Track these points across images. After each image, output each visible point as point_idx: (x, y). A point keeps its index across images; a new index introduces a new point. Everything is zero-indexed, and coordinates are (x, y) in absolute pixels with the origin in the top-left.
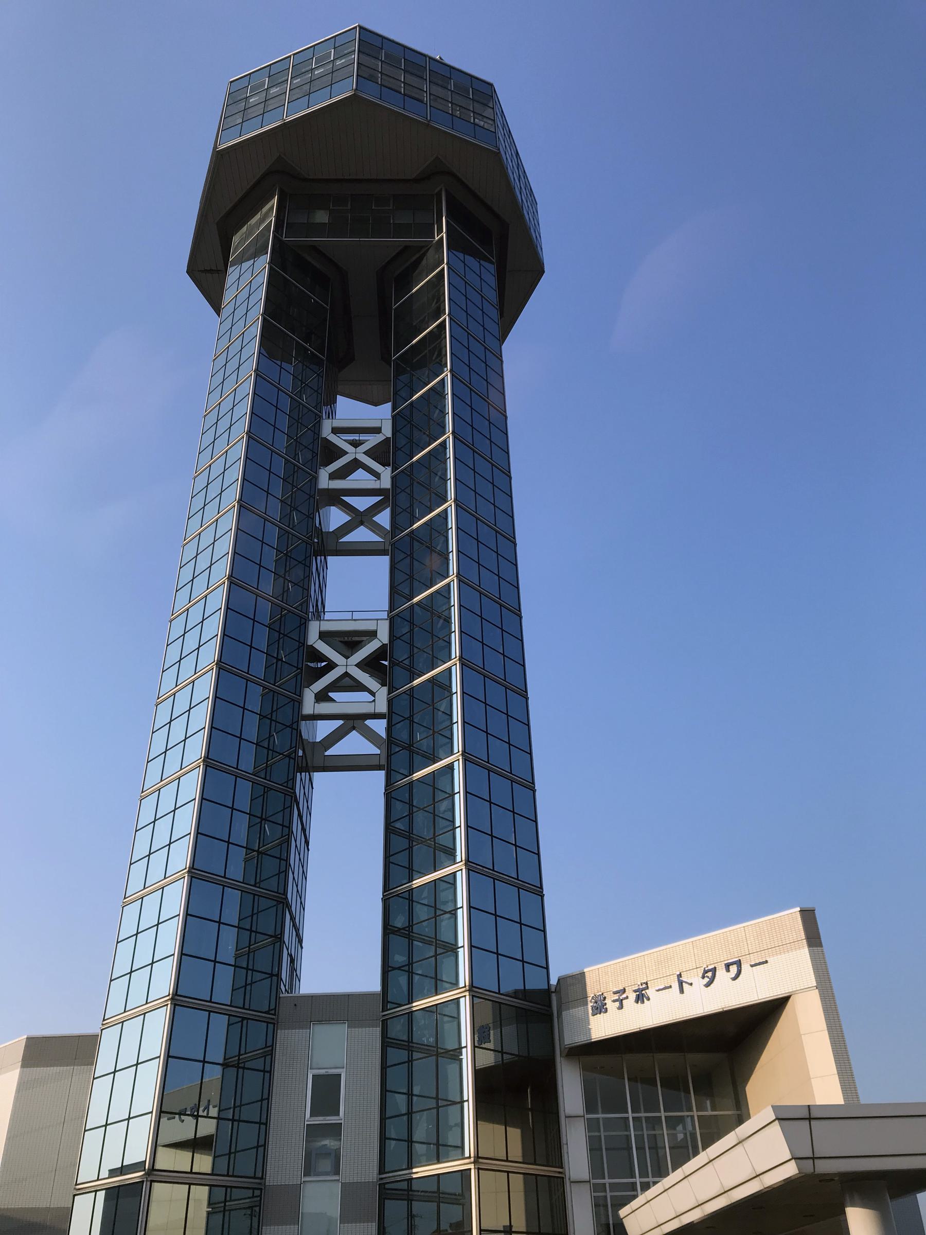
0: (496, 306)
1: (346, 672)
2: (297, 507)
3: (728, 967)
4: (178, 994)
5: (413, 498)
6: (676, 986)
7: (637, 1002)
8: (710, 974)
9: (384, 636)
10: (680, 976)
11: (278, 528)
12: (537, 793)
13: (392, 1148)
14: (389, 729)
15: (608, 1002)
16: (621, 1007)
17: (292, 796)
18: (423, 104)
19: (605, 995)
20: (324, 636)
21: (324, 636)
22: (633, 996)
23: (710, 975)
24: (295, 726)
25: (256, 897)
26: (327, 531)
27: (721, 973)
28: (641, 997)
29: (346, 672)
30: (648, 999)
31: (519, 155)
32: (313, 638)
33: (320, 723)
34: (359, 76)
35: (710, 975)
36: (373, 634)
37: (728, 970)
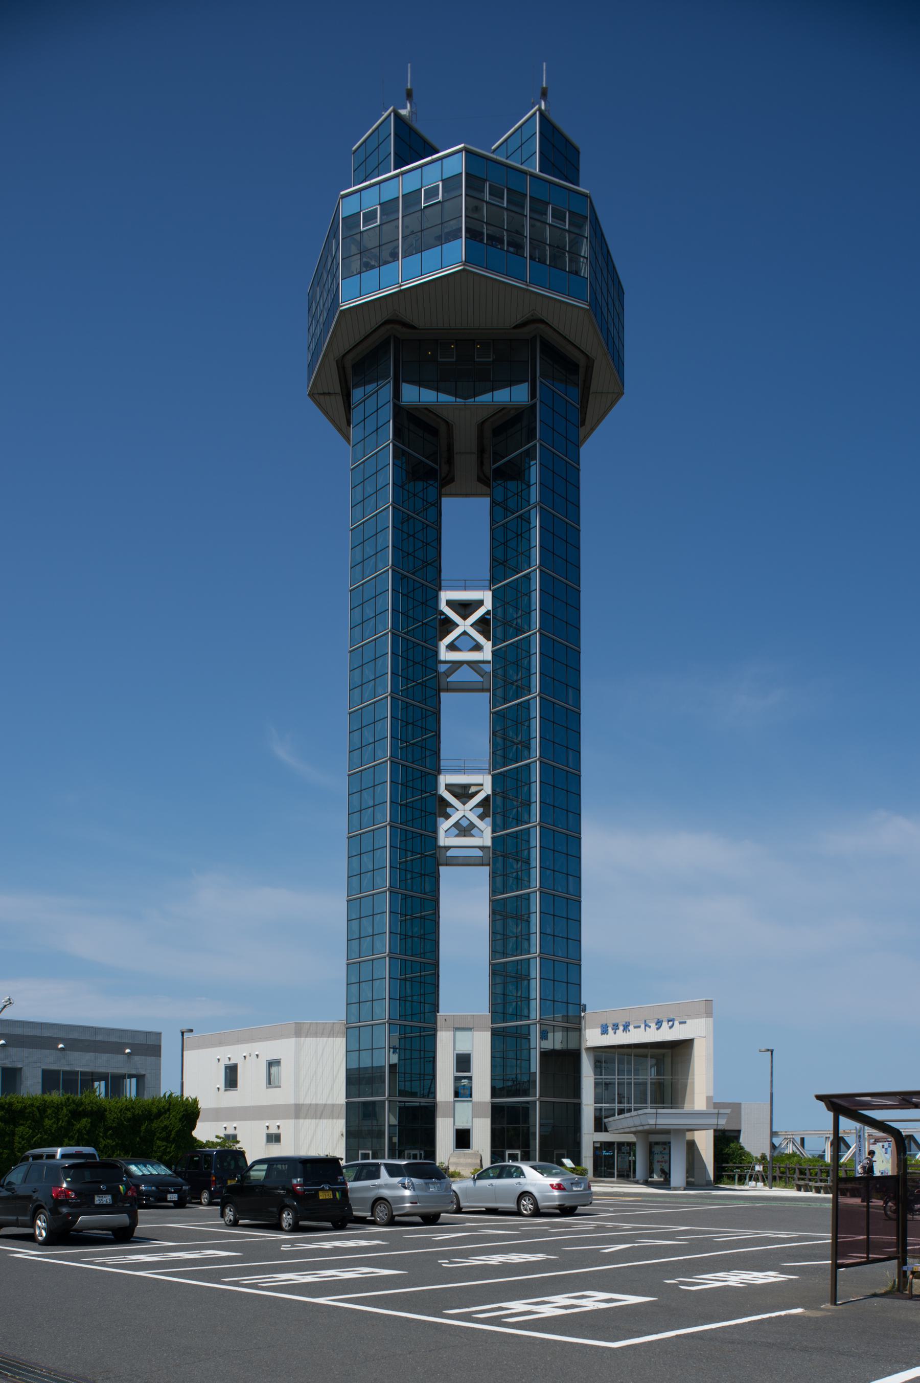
0: (576, 405)
1: (464, 805)
2: (418, 493)
3: (669, 1021)
5: (507, 528)
6: (643, 1026)
7: (623, 1032)
8: (660, 1024)
10: (645, 1021)
11: (400, 701)
12: (582, 777)
13: (502, 1320)
15: (610, 1029)
16: (615, 1033)
17: (435, 902)
18: (503, 251)
19: (608, 1025)
20: (449, 603)
22: (621, 1028)
25: (423, 900)
26: (443, 583)
27: (665, 1024)
29: (464, 805)
31: (610, 255)
34: (392, 978)
35: (659, 1024)
36: (480, 603)
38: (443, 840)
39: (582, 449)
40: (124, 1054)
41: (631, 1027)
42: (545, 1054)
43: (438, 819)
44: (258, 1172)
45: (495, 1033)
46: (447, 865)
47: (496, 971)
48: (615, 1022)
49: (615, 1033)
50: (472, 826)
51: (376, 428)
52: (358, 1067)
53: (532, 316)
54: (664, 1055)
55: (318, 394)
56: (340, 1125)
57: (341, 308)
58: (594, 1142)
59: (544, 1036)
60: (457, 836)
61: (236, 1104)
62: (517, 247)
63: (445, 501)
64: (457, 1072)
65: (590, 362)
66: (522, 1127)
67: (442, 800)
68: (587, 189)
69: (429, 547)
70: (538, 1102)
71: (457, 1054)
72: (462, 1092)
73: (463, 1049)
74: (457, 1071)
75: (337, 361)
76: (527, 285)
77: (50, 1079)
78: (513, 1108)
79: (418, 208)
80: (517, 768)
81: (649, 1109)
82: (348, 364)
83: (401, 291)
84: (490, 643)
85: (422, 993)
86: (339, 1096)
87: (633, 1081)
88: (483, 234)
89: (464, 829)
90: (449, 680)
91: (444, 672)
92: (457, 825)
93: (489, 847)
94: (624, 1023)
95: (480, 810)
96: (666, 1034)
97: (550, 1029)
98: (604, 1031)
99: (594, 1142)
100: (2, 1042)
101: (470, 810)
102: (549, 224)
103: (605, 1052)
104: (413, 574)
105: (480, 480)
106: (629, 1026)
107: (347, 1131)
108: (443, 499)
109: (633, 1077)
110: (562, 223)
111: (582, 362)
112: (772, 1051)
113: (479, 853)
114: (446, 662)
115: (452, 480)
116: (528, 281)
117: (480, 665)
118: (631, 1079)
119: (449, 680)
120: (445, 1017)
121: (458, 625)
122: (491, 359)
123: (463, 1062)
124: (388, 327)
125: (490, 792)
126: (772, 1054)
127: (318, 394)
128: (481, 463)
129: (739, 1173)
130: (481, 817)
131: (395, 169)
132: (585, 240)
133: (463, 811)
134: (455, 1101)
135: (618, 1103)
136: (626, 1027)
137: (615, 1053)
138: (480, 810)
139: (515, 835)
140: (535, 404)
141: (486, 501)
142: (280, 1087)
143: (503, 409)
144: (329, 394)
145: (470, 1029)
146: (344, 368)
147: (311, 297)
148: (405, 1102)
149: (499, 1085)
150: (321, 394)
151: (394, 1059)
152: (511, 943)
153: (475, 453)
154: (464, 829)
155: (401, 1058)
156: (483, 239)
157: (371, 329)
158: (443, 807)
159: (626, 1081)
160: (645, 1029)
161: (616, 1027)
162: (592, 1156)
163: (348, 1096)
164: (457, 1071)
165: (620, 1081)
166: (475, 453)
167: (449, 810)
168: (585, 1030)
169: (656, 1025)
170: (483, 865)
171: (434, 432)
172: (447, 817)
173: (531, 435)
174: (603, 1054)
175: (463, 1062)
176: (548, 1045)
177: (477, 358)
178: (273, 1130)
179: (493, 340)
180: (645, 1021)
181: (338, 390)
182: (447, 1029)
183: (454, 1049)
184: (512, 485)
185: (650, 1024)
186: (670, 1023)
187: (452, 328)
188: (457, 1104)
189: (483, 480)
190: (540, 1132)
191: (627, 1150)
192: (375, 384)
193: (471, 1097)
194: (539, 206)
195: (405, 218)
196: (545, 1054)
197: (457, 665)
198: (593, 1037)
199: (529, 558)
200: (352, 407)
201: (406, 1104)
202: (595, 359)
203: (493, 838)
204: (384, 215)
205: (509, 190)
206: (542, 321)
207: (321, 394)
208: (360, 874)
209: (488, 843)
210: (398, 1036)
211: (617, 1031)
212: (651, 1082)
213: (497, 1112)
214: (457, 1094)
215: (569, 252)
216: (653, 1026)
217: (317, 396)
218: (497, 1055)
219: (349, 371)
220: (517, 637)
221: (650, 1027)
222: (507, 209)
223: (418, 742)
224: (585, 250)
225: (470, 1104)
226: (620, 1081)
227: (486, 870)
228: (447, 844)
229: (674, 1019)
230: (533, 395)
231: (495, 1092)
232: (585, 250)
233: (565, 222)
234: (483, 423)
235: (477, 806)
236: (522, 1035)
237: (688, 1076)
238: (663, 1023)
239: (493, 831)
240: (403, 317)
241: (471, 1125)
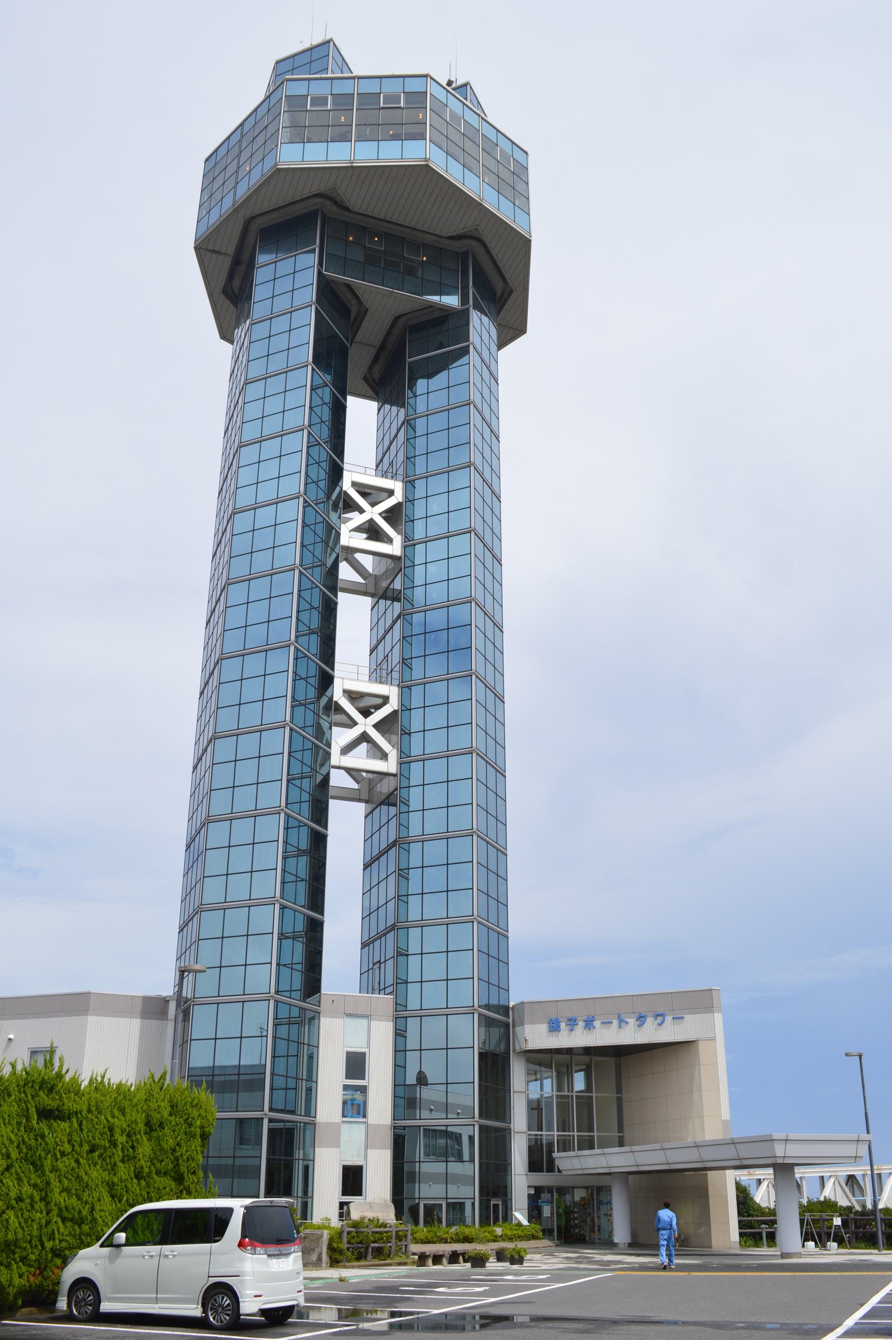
6: (615, 1022)
15: (563, 1025)
22: (581, 1024)
27: (650, 1020)
41: (597, 1024)
44: (861, 1256)
48: (570, 1015)
52: (212, 1065)
53: (470, 232)
55: (206, 249)
57: (278, 167)
66: (285, 1160)
71: (348, 1053)
73: (358, 1047)
74: (347, 1078)
82: (254, 227)
83: (352, 167)
94: (586, 1018)
98: (554, 1027)
112: (860, 1056)
121: (380, 514)
124: (319, 200)
126: (860, 1059)
127: (206, 249)
129: (767, 1230)
136: (589, 1024)
143: (431, 307)
144: (219, 253)
150: (209, 251)
153: (376, 347)
157: (300, 196)
161: (572, 1023)
162: (527, 1208)
164: (347, 1078)
166: (376, 347)
168: (514, 1027)
182: (334, 1015)
186: (658, 1018)
187: (387, 219)
192: (274, 256)
200: (257, 266)
201: (286, 1124)
202: (514, 290)
207: (209, 251)
211: (575, 1027)
216: (632, 1021)
217: (203, 252)
221: (627, 1023)
238: (648, 1019)
240: (341, 194)
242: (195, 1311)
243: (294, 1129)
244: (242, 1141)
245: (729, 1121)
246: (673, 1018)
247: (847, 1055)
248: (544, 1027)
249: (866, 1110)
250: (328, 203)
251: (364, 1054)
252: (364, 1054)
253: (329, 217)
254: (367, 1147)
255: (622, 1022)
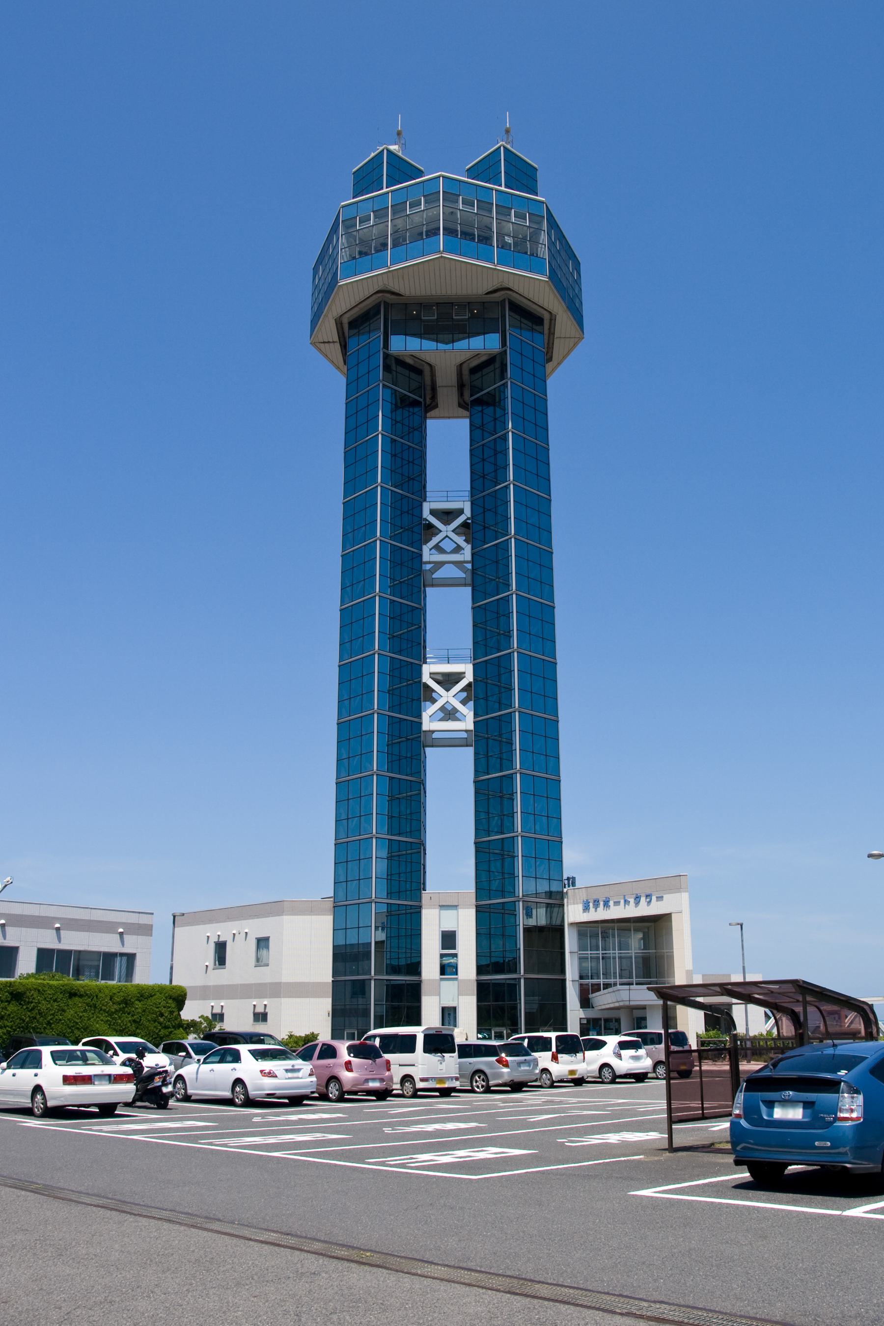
4: (674, 1146)
6: (622, 902)
8: (638, 899)
9: (468, 513)
10: (624, 896)
14: (473, 566)
15: (591, 905)
16: (596, 911)
20: (433, 512)
21: (433, 512)
22: (602, 903)
23: (637, 899)
24: (394, 422)
27: (643, 899)
28: (606, 904)
30: (588, 912)
32: (426, 514)
33: (427, 565)
35: (637, 899)
36: (461, 512)
37: (646, 899)
38: (427, 724)
39: (548, 382)
40: (116, 934)
41: (611, 903)
42: (528, 930)
43: (423, 703)
45: (479, 910)
46: (432, 746)
47: (480, 849)
48: (595, 897)
49: (596, 911)
50: (455, 710)
51: (368, 356)
54: (648, 928)
56: (326, 1004)
58: (580, 1019)
59: (529, 914)
60: (441, 720)
61: (268, 979)
62: (485, 240)
63: (430, 423)
64: (442, 949)
65: (553, 318)
67: (426, 686)
68: (543, 198)
69: (415, 416)
70: (522, 981)
71: (442, 931)
72: (447, 969)
73: (448, 927)
74: (443, 948)
75: (335, 320)
76: (496, 266)
77: (44, 956)
78: (499, 984)
79: (405, 243)
80: (499, 657)
81: (634, 986)
82: (345, 321)
84: (470, 546)
85: (408, 870)
86: (324, 972)
87: (617, 955)
88: (457, 231)
89: (449, 714)
90: (434, 576)
91: (429, 570)
92: (442, 709)
93: (472, 731)
95: (465, 694)
96: (644, 910)
97: (533, 906)
98: (586, 908)
99: (580, 1019)
100: (3, 921)
101: (453, 697)
102: (512, 223)
103: (590, 927)
104: (402, 438)
105: (460, 406)
106: (609, 901)
107: (333, 1010)
108: (427, 589)
109: (617, 952)
110: (524, 221)
111: (546, 317)
112: (742, 926)
113: (465, 735)
114: (429, 563)
115: (436, 406)
116: (496, 262)
117: (465, 564)
118: (599, 954)
119: (434, 576)
120: (430, 895)
122: (467, 317)
123: (449, 939)
124: (380, 295)
125: (472, 680)
128: (461, 394)
130: (464, 702)
131: (387, 188)
132: (543, 232)
133: (448, 697)
134: (442, 979)
135: (599, 978)
137: (598, 927)
138: (465, 694)
139: (498, 718)
140: (505, 351)
141: (467, 422)
142: (267, 965)
144: (329, 342)
145: (455, 907)
146: (341, 324)
147: (315, 269)
148: (406, 980)
149: (485, 962)
150: (321, 343)
151: (382, 936)
152: (495, 821)
154: (449, 714)
155: (388, 935)
156: (457, 235)
158: (429, 695)
159: (612, 955)
160: (625, 906)
161: (596, 903)
163: (334, 974)
164: (443, 948)
165: (592, 955)
167: (434, 695)
168: (568, 906)
169: (635, 900)
170: (467, 746)
171: (419, 372)
172: (434, 701)
173: (503, 376)
174: (588, 929)
175: (449, 939)
176: (532, 922)
177: (455, 316)
178: (260, 1009)
179: (469, 303)
180: (624, 896)
181: (336, 339)
182: (431, 907)
183: (440, 927)
184: (489, 410)
185: (629, 900)
188: (443, 983)
189: (463, 405)
190: (525, 1009)
191: (615, 1026)
193: (457, 974)
194: (504, 211)
195: (393, 221)
196: (528, 930)
197: (439, 565)
198: (574, 913)
199: (506, 455)
203: (474, 722)
204: (376, 218)
205: (477, 200)
206: (509, 289)
208: (349, 739)
209: (471, 727)
210: (386, 914)
212: (635, 956)
213: (483, 991)
214: (443, 972)
215: (529, 241)
217: (318, 345)
218: (482, 931)
219: (346, 327)
220: (486, 599)
222: (477, 214)
223: (405, 581)
224: (544, 238)
225: (456, 982)
226: (592, 955)
227: (470, 751)
228: (432, 728)
229: (651, 894)
230: (504, 344)
231: (480, 970)
232: (544, 238)
233: (526, 220)
234: (461, 365)
235: (462, 690)
236: (508, 911)
237: (673, 949)
239: (476, 715)
241: (457, 1003)
242: (227, 1094)
243: (516, 984)
244: (354, 994)
245: (692, 970)
246: (657, 897)
247: (730, 924)
248: (580, 907)
249: (744, 964)
250: (388, 295)
251: (455, 931)
252: (455, 931)
253: (391, 304)
254: (458, 995)
255: (626, 902)
